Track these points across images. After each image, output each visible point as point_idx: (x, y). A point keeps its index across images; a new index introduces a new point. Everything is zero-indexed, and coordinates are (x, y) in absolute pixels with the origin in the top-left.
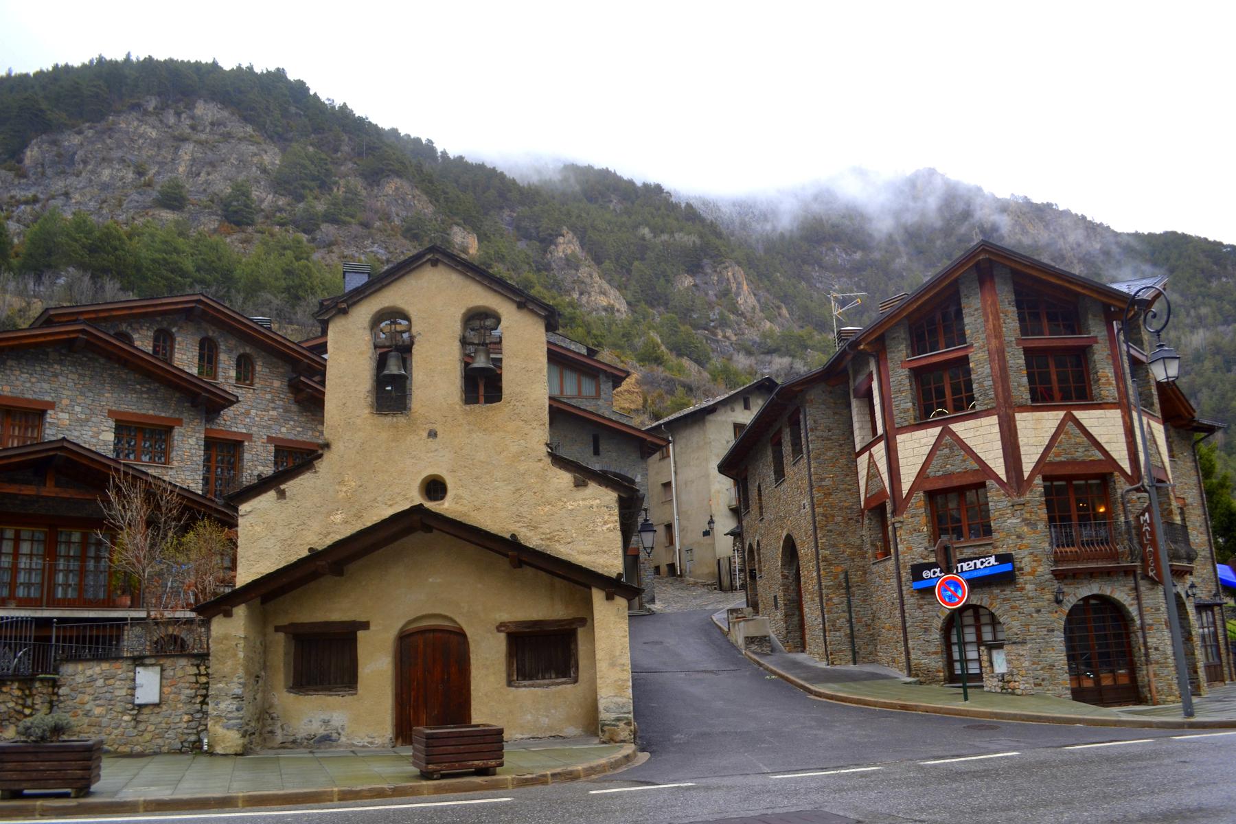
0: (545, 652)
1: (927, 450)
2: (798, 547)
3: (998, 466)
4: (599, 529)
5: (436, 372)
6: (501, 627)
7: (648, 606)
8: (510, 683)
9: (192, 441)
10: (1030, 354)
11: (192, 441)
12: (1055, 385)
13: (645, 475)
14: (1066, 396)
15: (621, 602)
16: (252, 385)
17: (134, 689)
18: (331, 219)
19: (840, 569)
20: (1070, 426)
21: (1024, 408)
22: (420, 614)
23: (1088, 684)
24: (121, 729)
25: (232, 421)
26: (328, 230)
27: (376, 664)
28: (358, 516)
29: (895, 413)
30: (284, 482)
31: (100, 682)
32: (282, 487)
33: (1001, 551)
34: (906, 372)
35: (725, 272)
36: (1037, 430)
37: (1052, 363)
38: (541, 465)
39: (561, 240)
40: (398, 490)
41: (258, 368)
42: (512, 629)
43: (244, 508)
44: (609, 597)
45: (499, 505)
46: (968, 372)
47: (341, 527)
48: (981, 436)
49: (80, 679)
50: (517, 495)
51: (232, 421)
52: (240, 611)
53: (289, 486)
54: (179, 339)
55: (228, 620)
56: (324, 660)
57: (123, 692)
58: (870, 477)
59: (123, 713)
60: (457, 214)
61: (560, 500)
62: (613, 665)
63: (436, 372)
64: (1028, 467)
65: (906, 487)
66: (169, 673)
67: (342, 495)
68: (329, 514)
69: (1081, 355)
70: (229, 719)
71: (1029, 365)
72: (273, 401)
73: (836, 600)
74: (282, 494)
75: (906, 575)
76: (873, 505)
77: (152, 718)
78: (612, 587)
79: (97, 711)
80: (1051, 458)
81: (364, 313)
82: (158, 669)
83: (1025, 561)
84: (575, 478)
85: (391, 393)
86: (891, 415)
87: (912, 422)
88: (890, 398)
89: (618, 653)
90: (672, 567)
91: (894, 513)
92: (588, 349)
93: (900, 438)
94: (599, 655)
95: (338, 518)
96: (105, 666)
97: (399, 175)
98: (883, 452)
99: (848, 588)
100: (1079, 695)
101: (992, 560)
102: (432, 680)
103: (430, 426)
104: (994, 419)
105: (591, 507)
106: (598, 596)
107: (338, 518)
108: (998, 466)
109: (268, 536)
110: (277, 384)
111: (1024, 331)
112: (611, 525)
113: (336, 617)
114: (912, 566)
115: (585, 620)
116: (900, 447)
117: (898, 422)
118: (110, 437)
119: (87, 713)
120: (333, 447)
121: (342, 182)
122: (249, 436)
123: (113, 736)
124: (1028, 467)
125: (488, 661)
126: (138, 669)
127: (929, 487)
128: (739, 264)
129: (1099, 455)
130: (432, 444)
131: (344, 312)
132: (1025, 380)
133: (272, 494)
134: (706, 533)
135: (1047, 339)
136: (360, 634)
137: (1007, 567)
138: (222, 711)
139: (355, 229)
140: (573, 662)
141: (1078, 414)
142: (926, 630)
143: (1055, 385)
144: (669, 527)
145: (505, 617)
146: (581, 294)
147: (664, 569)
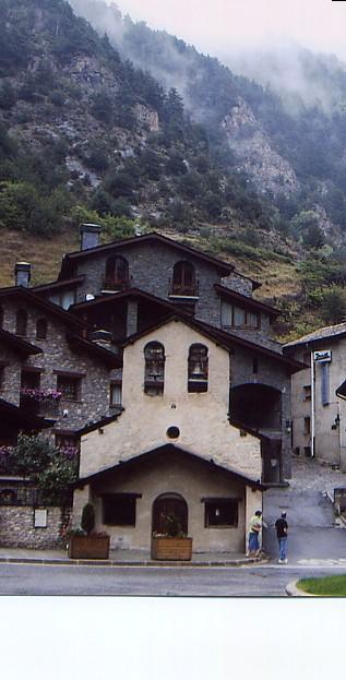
0: (224, 513)
5: (176, 374)
6: (203, 500)
7: (286, 480)
8: (206, 527)
9: (15, 375)
11: (15, 375)
13: (289, 388)
15: (259, 492)
16: (45, 338)
18: (27, 96)
25: (37, 362)
26: (23, 106)
27: (144, 514)
30: (103, 425)
39: (236, 109)
41: (49, 328)
43: (83, 438)
44: (254, 491)
47: (130, 451)
49: (8, 514)
51: (37, 362)
52: (87, 487)
54: (6, 311)
55: (81, 492)
56: (122, 514)
60: (140, 93)
63: (176, 374)
66: (51, 513)
72: (57, 348)
74: (101, 432)
78: (256, 486)
79: (16, 529)
81: (142, 344)
85: (154, 387)
90: (308, 449)
95: (128, 445)
96: (20, 508)
97: (88, 53)
102: (170, 520)
106: (248, 490)
107: (128, 445)
109: (98, 453)
110: (59, 337)
113: (125, 491)
115: (243, 499)
119: (12, 530)
121: (37, 59)
122: (43, 370)
125: (196, 514)
131: (132, 343)
133: (97, 431)
134: (334, 427)
136: (138, 500)
139: (48, 105)
144: (308, 420)
145: (205, 495)
146: (253, 164)
147: (302, 451)
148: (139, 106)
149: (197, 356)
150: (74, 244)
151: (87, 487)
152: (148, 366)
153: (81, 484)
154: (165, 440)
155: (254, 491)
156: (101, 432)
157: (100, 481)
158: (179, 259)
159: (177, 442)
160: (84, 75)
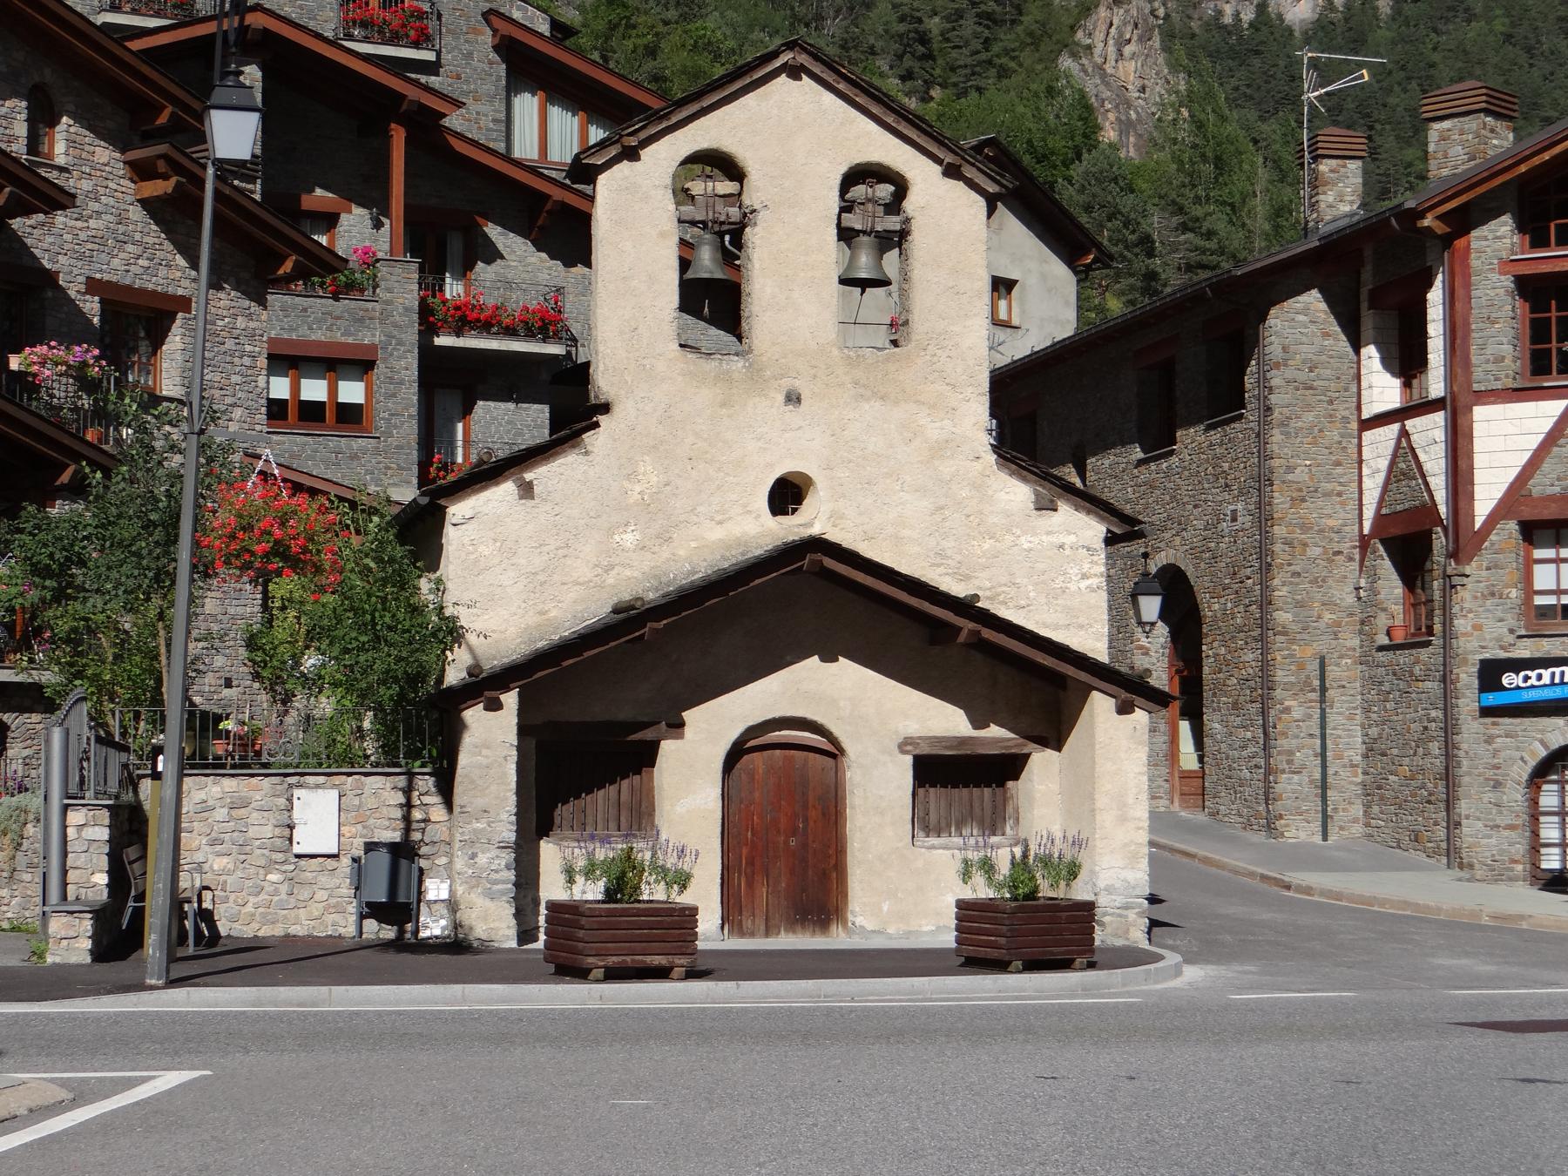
1: (1534, 442)
2: (1203, 598)
4: (1073, 587)
5: (791, 265)
17: (291, 827)
19: (1309, 652)
22: (777, 714)
24: (263, 896)
28: (665, 538)
29: (1474, 359)
31: (221, 813)
32: (528, 476)
34: (1507, 282)
38: (978, 466)
40: (734, 497)
42: (925, 750)
43: (458, 510)
44: (1124, 709)
45: (906, 533)
50: (938, 518)
53: (538, 475)
57: (268, 831)
58: (1395, 475)
59: (269, 867)
61: (1009, 531)
62: (1123, 819)
65: (1483, 508)
67: (634, 497)
68: (610, 532)
70: (496, 882)
73: (1297, 713)
74: (527, 490)
75: (1467, 677)
76: (1395, 531)
77: (323, 879)
79: (219, 863)
82: (334, 794)
84: (1037, 494)
86: (1467, 364)
87: (1511, 384)
88: (1467, 324)
89: (1131, 801)
91: (1454, 554)
92: (555, 25)
93: (1479, 412)
94: (1102, 801)
95: (629, 539)
98: (1440, 435)
99: (1323, 689)
103: (787, 383)
105: (1061, 547)
107: (629, 539)
109: (524, 566)
112: (1094, 582)
114: (1482, 662)
116: (1478, 430)
117: (1482, 376)
120: (617, 410)
123: (249, 908)
126: (297, 793)
127: (1529, 514)
130: (791, 414)
133: (506, 490)
138: (483, 869)
140: (1010, 810)
142: (1497, 785)
145: (914, 728)
149: (871, 216)
151: (510, 699)
155: (1124, 709)
156: (527, 490)
157: (543, 676)
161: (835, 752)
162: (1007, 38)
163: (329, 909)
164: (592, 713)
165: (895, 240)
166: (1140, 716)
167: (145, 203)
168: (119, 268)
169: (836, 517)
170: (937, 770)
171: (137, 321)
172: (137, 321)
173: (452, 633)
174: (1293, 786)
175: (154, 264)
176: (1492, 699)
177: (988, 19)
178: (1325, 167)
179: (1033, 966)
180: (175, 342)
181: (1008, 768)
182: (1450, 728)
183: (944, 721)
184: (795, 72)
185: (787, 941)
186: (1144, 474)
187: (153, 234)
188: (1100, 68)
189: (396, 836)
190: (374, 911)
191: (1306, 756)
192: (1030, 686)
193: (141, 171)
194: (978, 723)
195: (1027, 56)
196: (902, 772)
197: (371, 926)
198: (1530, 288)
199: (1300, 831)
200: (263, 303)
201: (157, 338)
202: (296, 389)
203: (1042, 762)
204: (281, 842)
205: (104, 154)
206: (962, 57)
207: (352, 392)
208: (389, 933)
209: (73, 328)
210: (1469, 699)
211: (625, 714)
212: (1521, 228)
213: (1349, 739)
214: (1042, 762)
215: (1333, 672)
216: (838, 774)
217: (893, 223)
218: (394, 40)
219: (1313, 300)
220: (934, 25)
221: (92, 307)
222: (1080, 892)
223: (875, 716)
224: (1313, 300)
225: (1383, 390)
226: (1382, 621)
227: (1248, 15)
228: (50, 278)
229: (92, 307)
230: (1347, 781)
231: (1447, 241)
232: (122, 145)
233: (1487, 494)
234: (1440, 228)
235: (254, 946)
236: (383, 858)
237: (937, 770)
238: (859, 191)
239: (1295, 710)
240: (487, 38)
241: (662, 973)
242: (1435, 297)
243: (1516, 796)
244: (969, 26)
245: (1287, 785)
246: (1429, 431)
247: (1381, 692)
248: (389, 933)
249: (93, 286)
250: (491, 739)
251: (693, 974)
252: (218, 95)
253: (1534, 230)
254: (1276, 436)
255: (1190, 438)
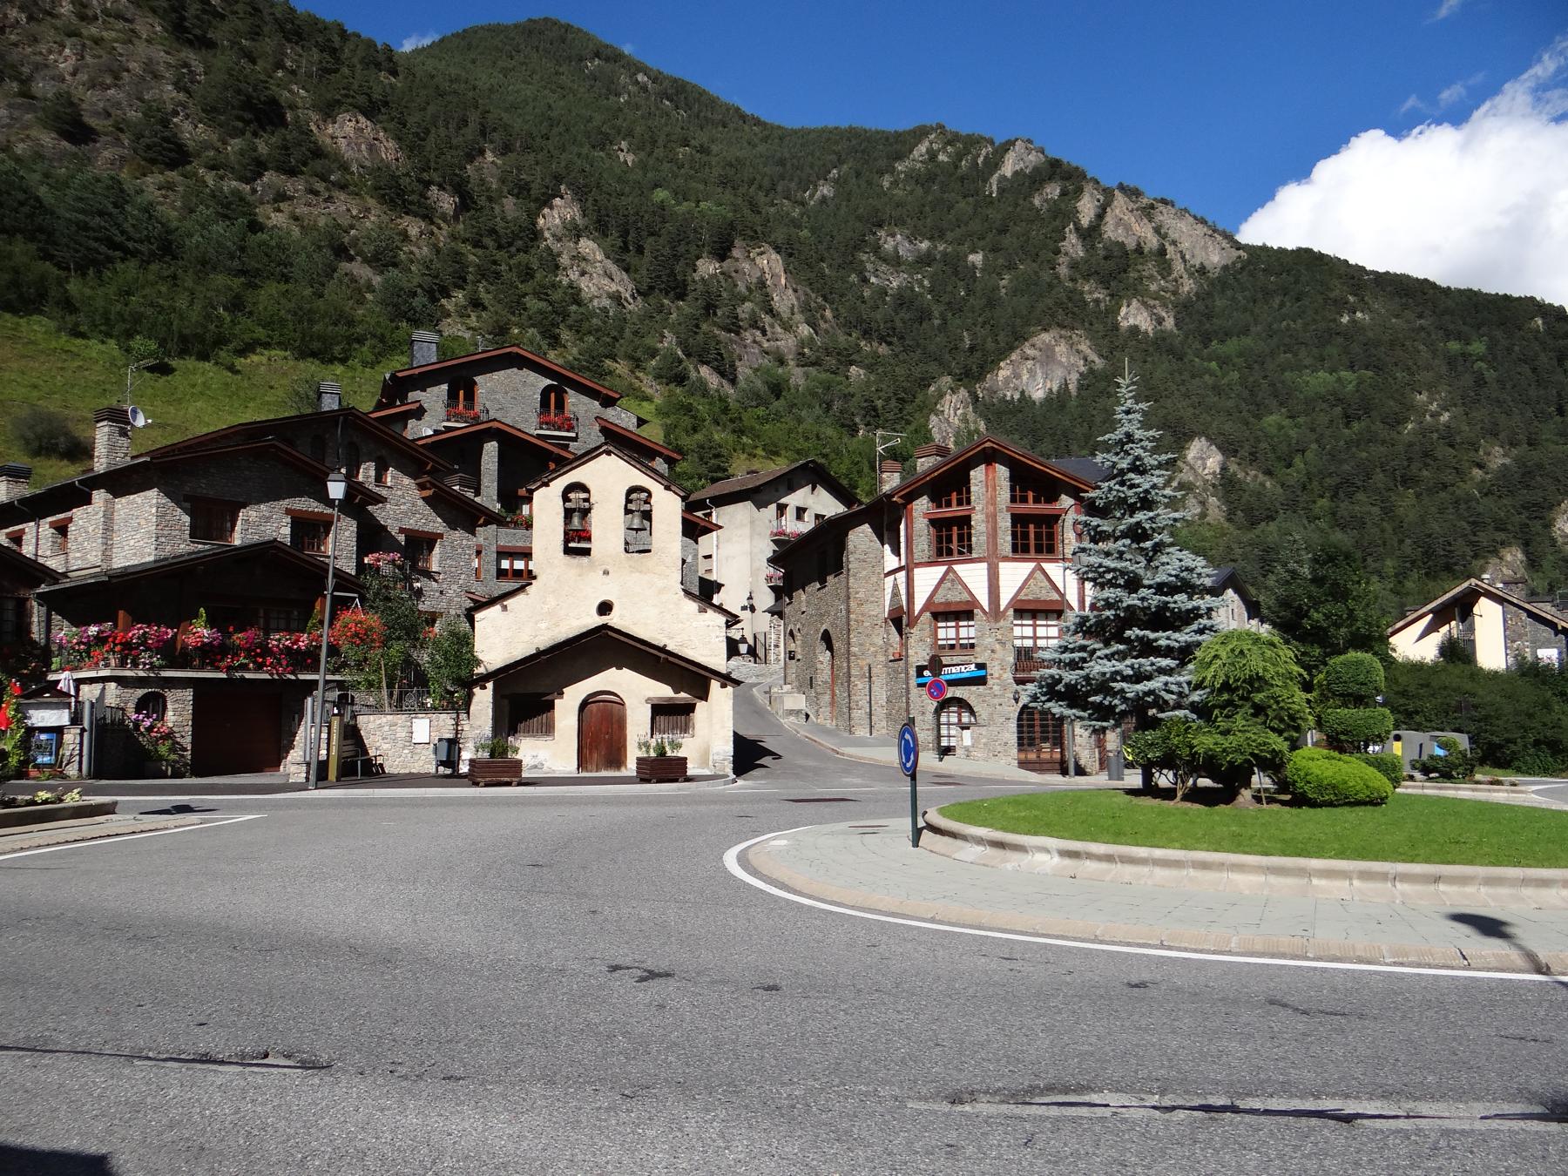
1: (935, 582)
3: (983, 598)
5: (608, 524)
10: (1017, 519)
12: (1032, 542)
14: (1039, 550)
20: (1038, 574)
21: (1006, 559)
23: (1032, 756)
33: (979, 661)
35: (758, 260)
36: (1014, 575)
37: (1032, 526)
44: (723, 686)
46: (970, 527)
48: (974, 576)
49: (371, 726)
52: (490, 685)
53: (509, 602)
64: (1004, 601)
69: (1053, 519)
71: (1014, 525)
74: (505, 608)
75: (913, 672)
79: (385, 746)
80: (1022, 597)
81: (560, 484)
83: (994, 670)
85: (576, 542)
93: (916, 571)
95: (543, 625)
100: (1023, 764)
101: (973, 667)
104: (985, 565)
107: (543, 625)
108: (983, 598)
109: (502, 638)
111: (1013, 499)
116: (916, 578)
118: (287, 531)
124: (1004, 601)
128: (778, 249)
129: (1056, 597)
132: (1009, 538)
133: (498, 608)
135: (1031, 507)
137: (982, 673)
141: (1044, 565)
143: (1032, 542)
145: (652, 695)
148: (1078, 725)
149: (637, 506)
150: (610, 373)
151: (490, 685)
152: (568, 514)
153: (482, 681)
154: (599, 621)
155: (723, 686)
156: (505, 608)
157: (506, 678)
158: (548, 382)
159: (614, 620)
160: (579, 258)
161: (623, 704)
162: (909, 408)
163: (426, 763)
164: (526, 692)
165: (647, 515)
166: (729, 689)
167: (423, 499)
168: (412, 523)
169: (622, 617)
170: (660, 710)
171: (419, 544)
172: (419, 544)
173: (478, 662)
174: (859, 714)
175: (429, 521)
176: (921, 680)
177: (901, 400)
178: (884, 476)
179: (660, 781)
180: (437, 550)
181: (689, 709)
182: (908, 692)
183: (664, 691)
184: (609, 453)
185: (604, 773)
186: (820, 594)
187: (428, 510)
188: (947, 420)
189: (451, 736)
190: (442, 763)
191: (864, 703)
192: (692, 679)
193: (421, 487)
194: (676, 692)
195: (917, 415)
196: (647, 712)
197: (441, 769)
198: (934, 523)
199: (862, 732)
200: (474, 534)
201: (431, 549)
202: (512, 564)
203: (700, 705)
204: (404, 737)
205: (407, 481)
206: (890, 416)
207: (519, 565)
208: (449, 771)
209: (392, 545)
210: (914, 681)
211: (541, 690)
212: (932, 500)
213: (881, 695)
214: (701, 706)
215: (874, 671)
216: (624, 711)
217: (647, 507)
218: (559, 429)
219: (866, 528)
220: (879, 403)
221: (402, 538)
222: (518, 757)
223: (636, 691)
224: (866, 528)
225: (891, 561)
226: (891, 650)
227: (1017, 396)
228: (384, 528)
229: (402, 538)
230: (880, 713)
231: (905, 506)
232: (414, 476)
233: (919, 604)
234: (900, 501)
235: (391, 776)
236: (445, 744)
237: (660, 710)
238: (634, 496)
239: (860, 685)
240: (597, 427)
241: (509, 784)
242: (902, 527)
243: (930, 717)
244: (893, 403)
245: (856, 714)
246: (902, 576)
247: (892, 677)
248: (449, 771)
249: (402, 530)
250: (483, 699)
251: (520, 784)
252: (331, 476)
253: (937, 500)
254: (851, 580)
255: (830, 578)
